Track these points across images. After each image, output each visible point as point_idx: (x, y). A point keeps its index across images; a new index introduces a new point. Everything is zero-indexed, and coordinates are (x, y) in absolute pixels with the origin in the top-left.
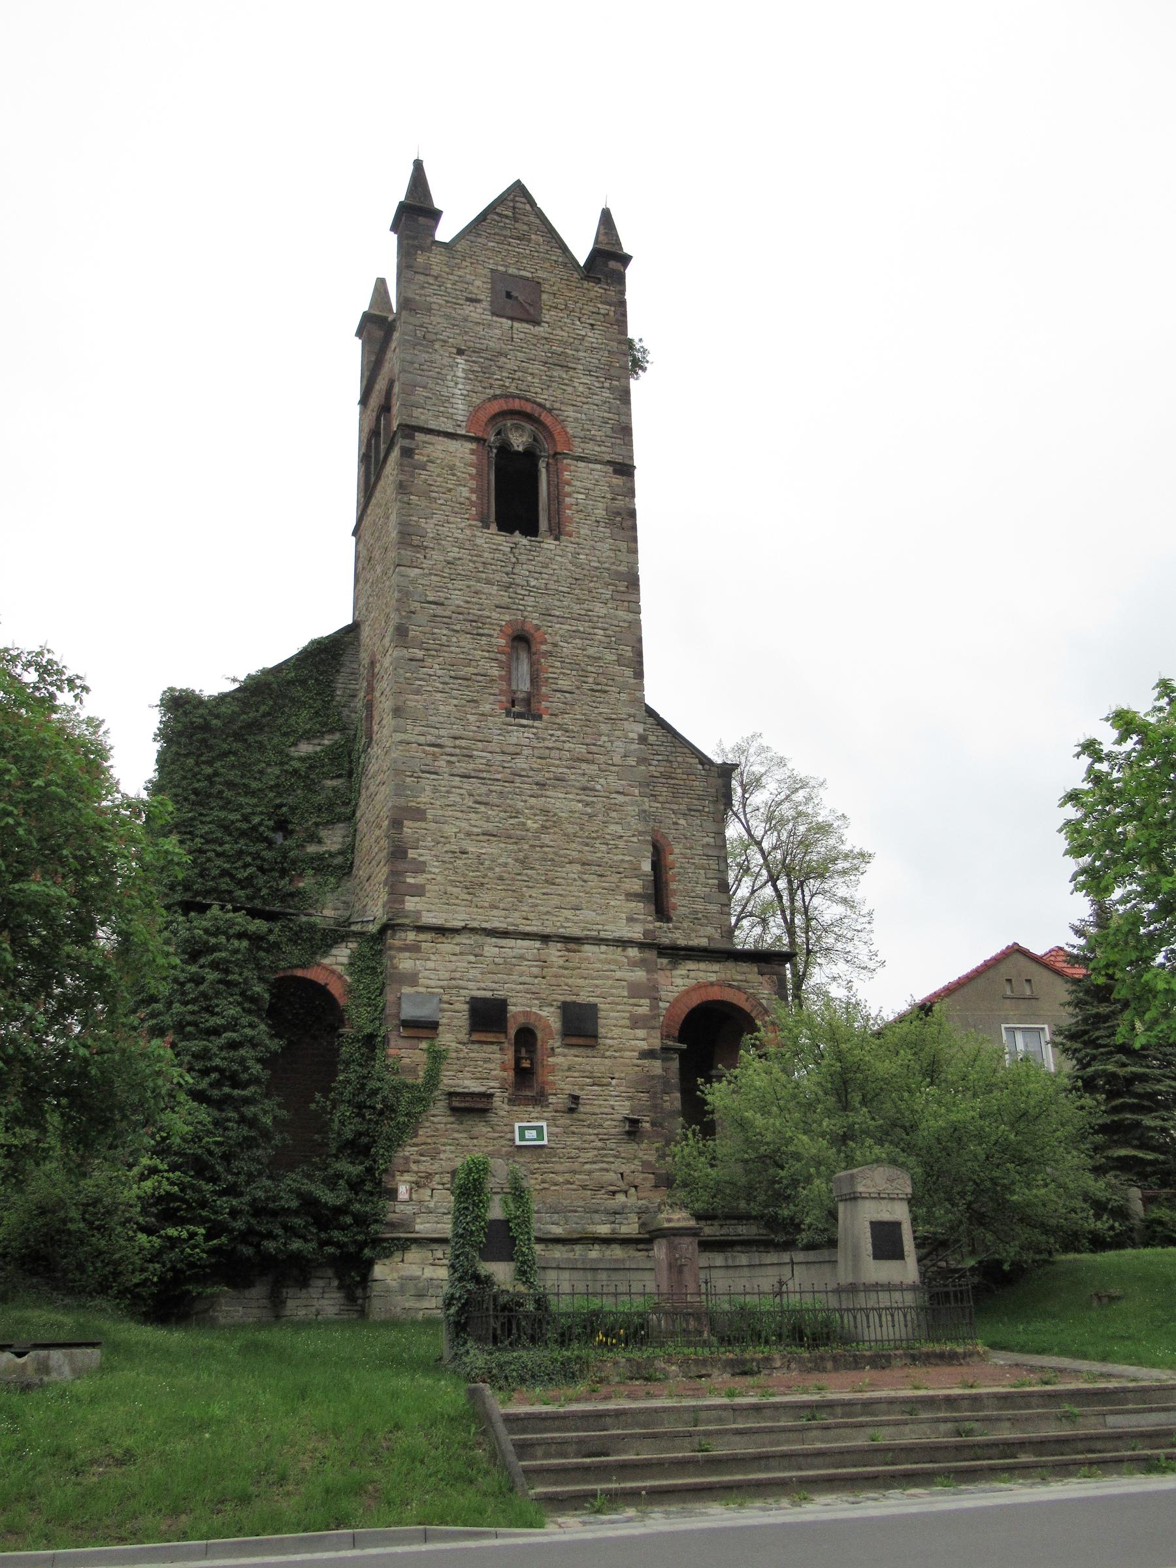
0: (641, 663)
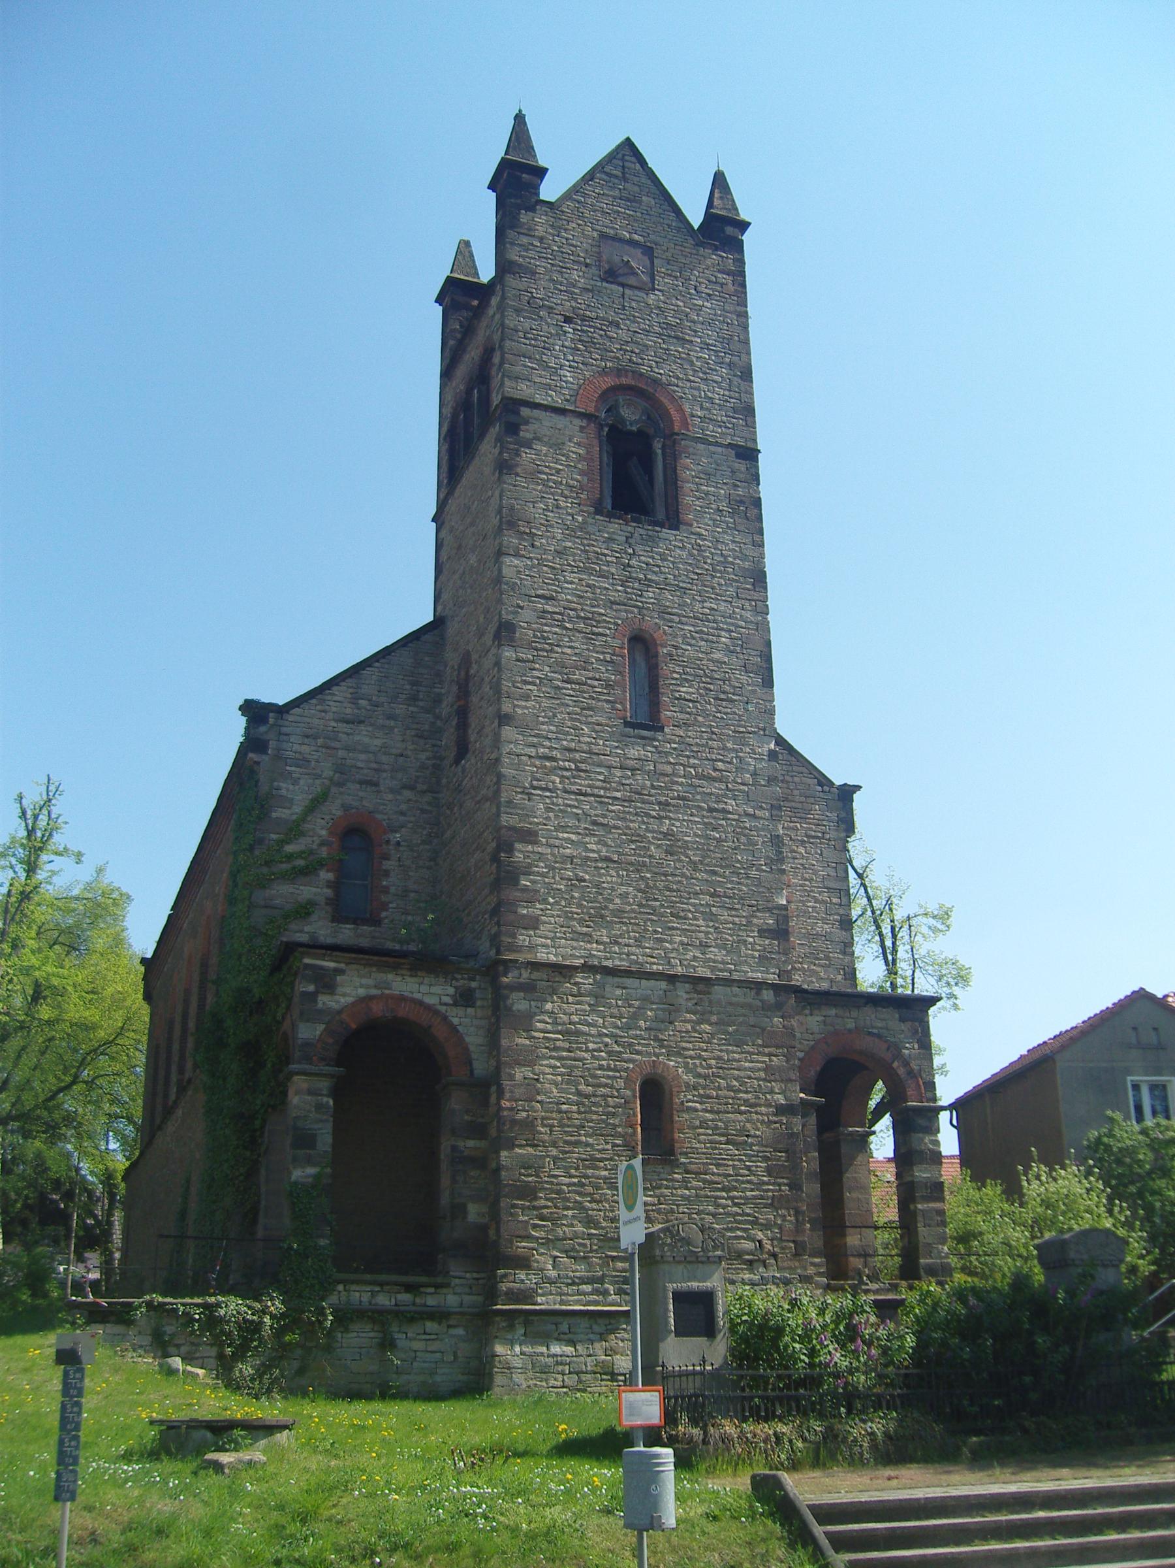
0: (770, 669)
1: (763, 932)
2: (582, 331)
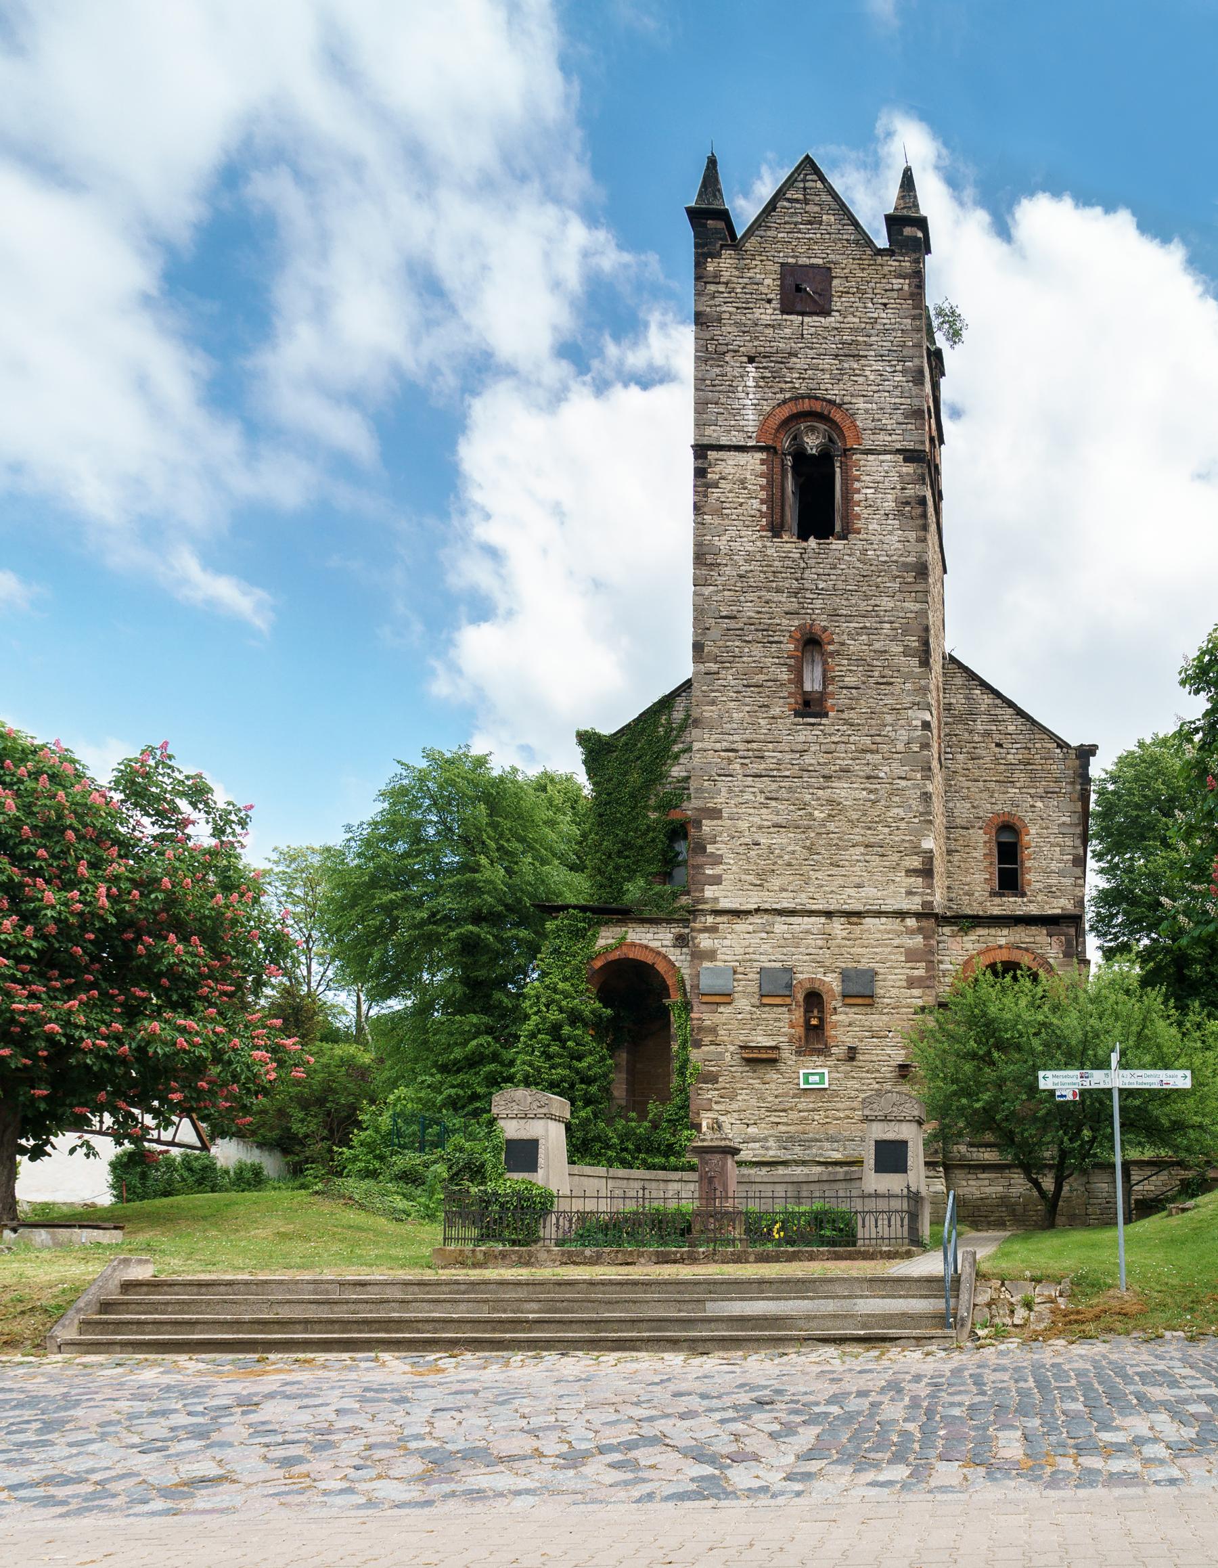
2: (764, 368)
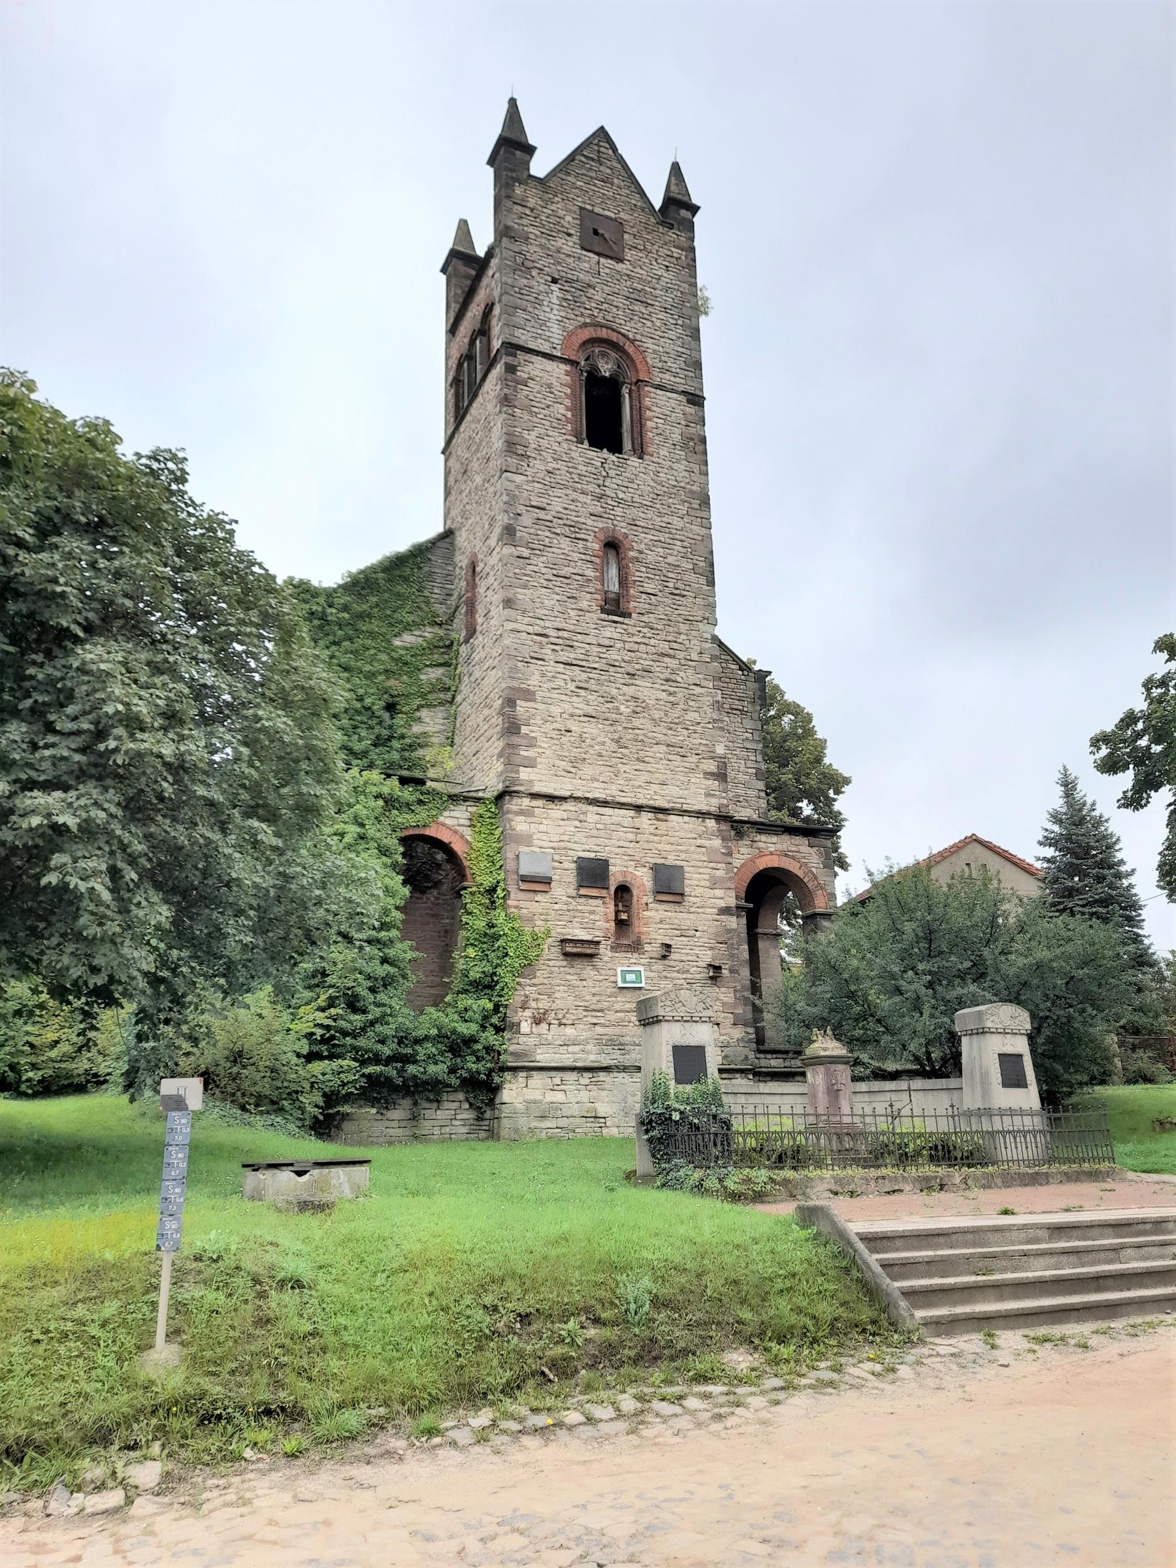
1: (708, 775)
